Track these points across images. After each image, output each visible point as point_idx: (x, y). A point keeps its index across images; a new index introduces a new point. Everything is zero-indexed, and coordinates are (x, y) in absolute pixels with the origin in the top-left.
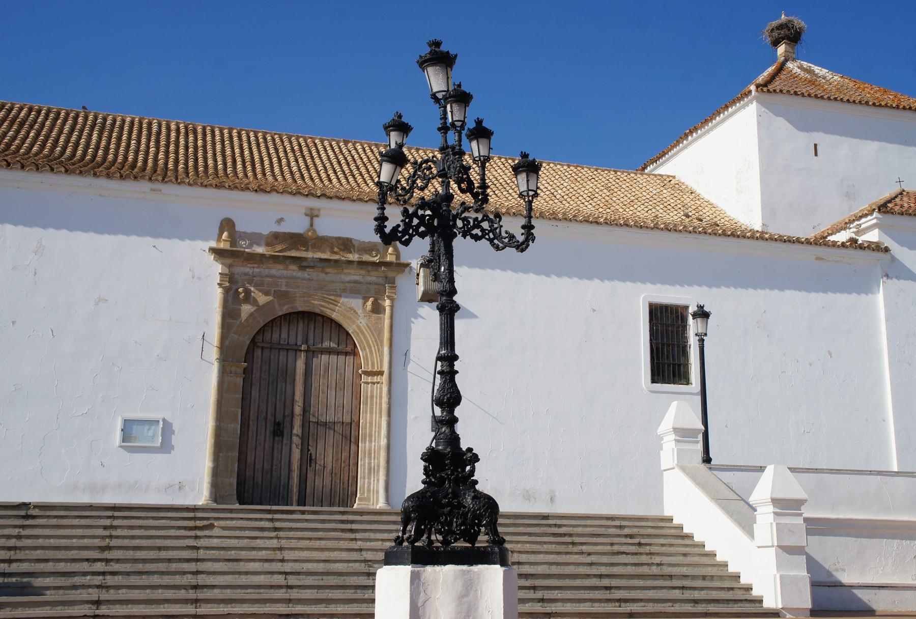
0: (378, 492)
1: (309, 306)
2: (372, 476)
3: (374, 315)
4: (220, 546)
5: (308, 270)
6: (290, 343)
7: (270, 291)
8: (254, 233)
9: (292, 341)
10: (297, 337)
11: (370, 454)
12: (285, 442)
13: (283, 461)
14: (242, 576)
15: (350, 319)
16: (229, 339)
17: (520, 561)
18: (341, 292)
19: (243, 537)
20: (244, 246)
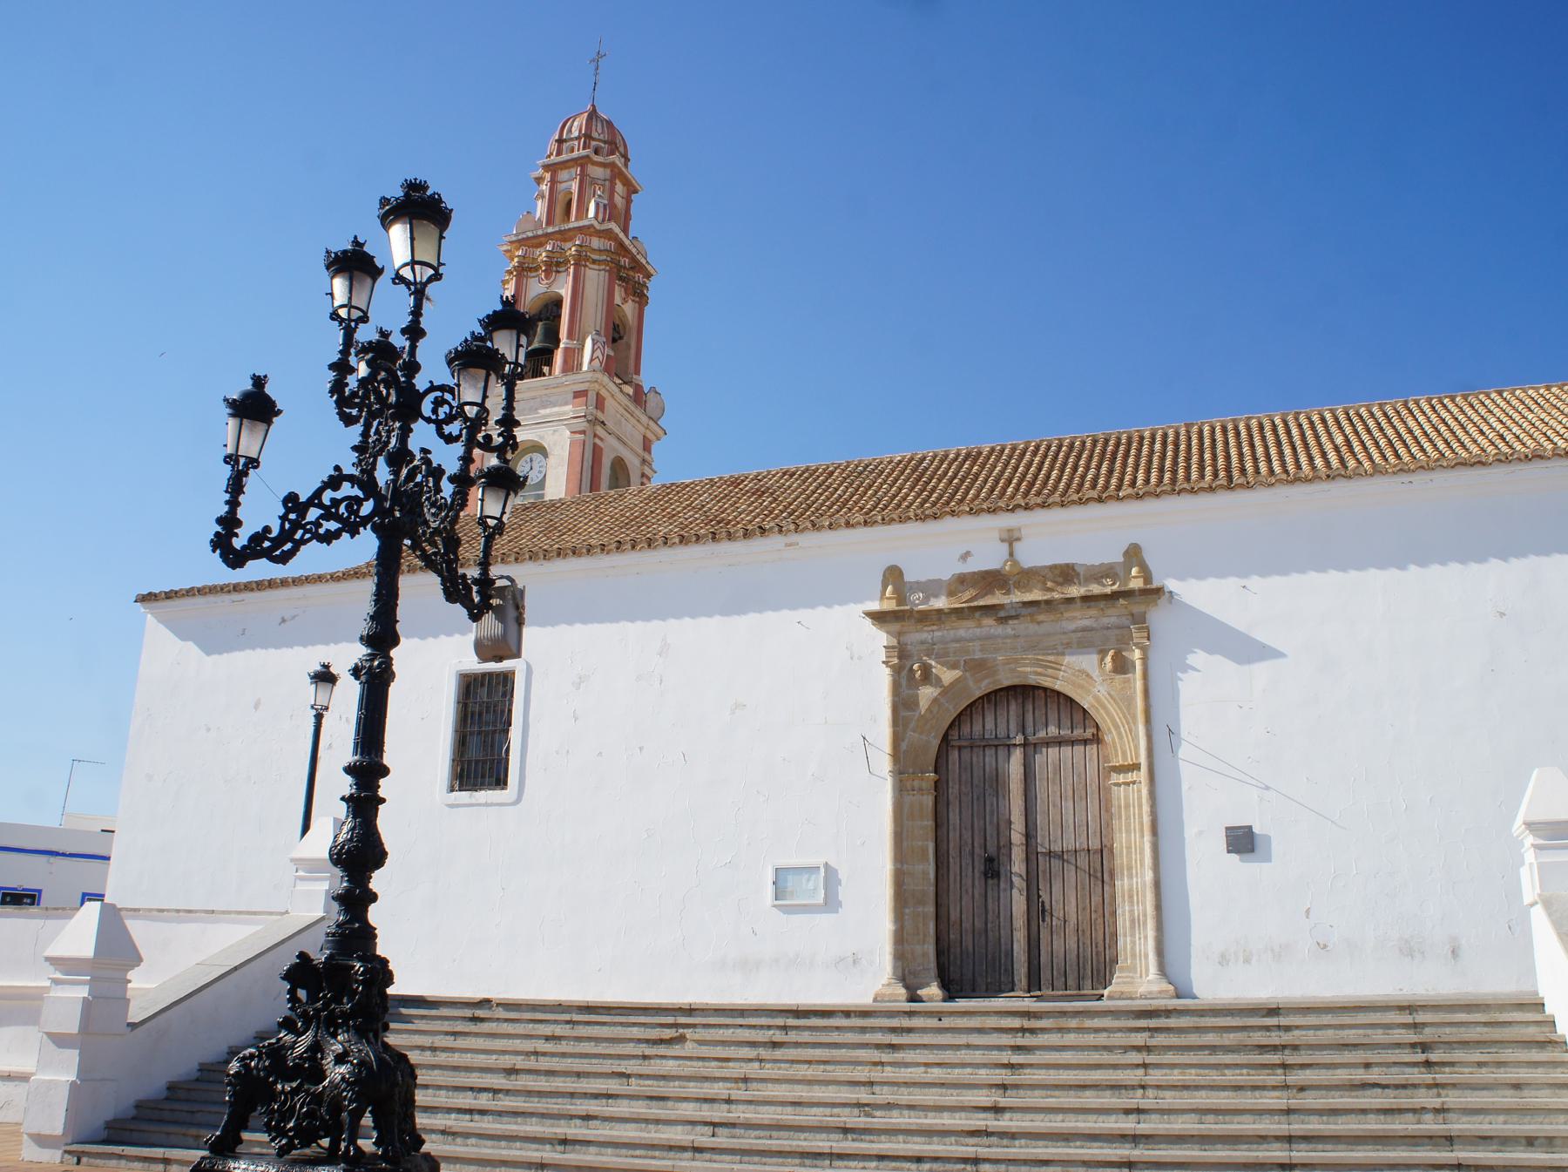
0: (1146, 956)
2: (1137, 932)
3: (1118, 677)
4: (657, 1073)
5: (1010, 622)
6: (999, 736)
7: (959, 661)
9: (1002, 733)
11: (1131, 897)
12: (1002, 885)
13: (1001, 914)
14: (650, 1126)
15: (1082, 687)
16: (906, 741)
17: (1140, 1107)
19: (709, 1058)
20: (917, 602)
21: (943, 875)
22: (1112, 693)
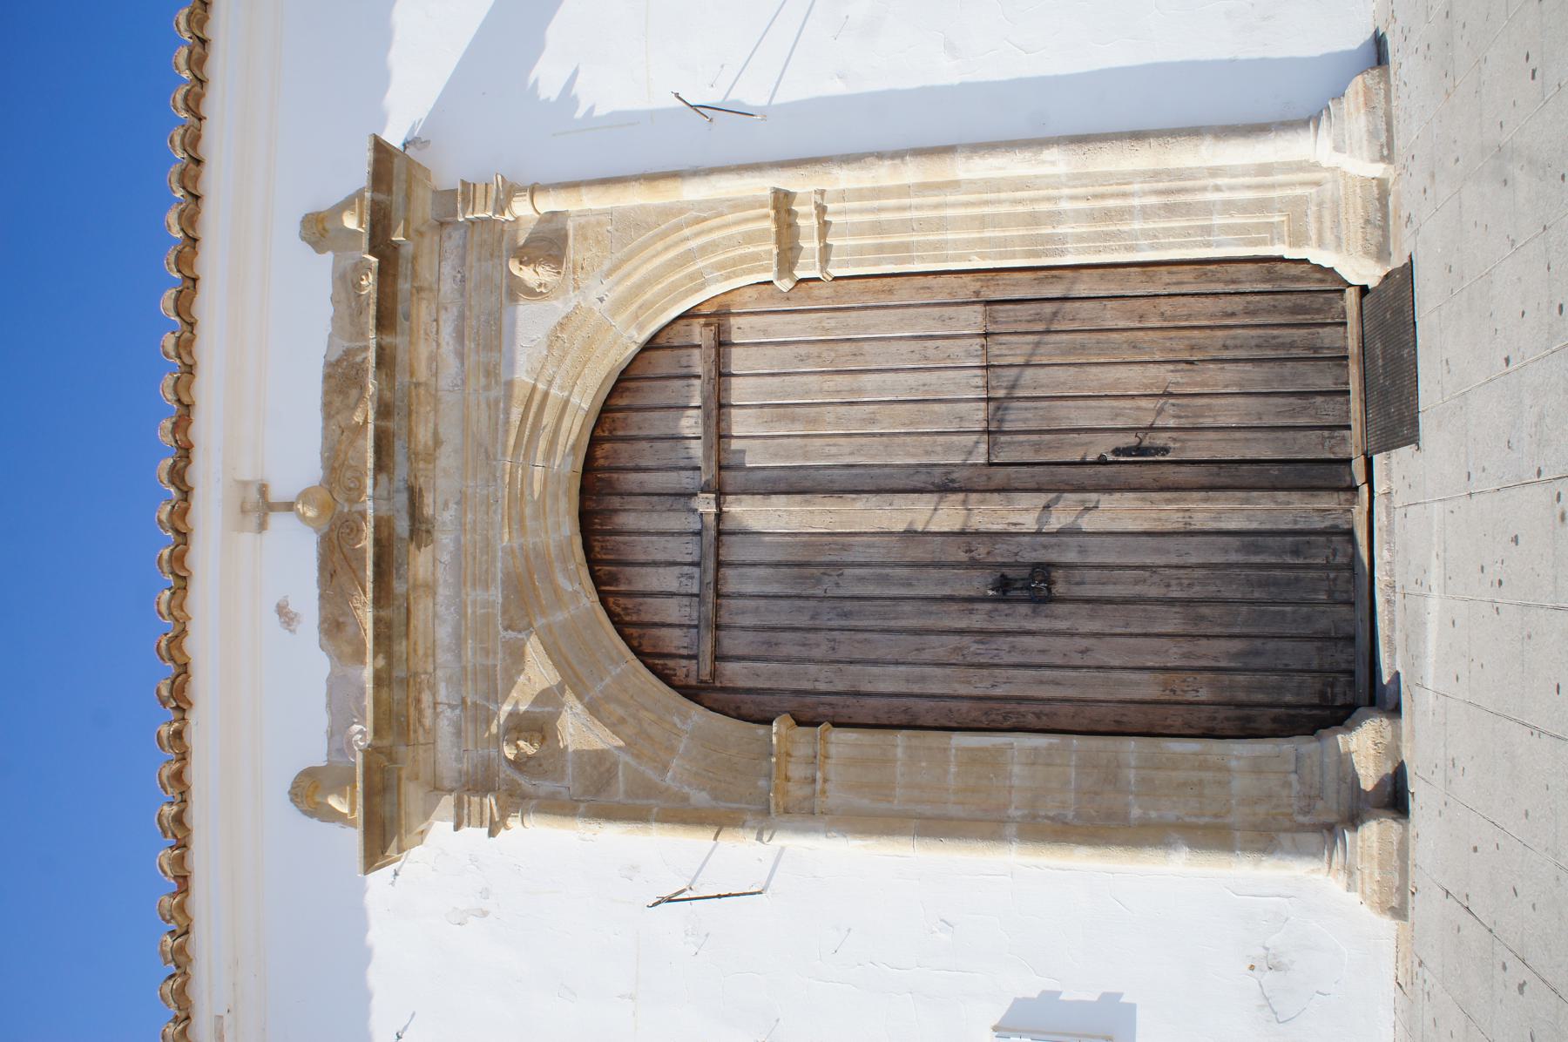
0: (1264, 169)
1: (556, 498)
2: (1199, 197)
5: (428, 511)
6: (696, 559)
7: (506, 643)
8: (329, 705)
10: (673, 534)
11: (1107, 215)
12: (1071, 557)
13: (1148, 561)
16: (686, 789)
18: (496, 382)
21: (1038, 715)
22: (607, 265)
